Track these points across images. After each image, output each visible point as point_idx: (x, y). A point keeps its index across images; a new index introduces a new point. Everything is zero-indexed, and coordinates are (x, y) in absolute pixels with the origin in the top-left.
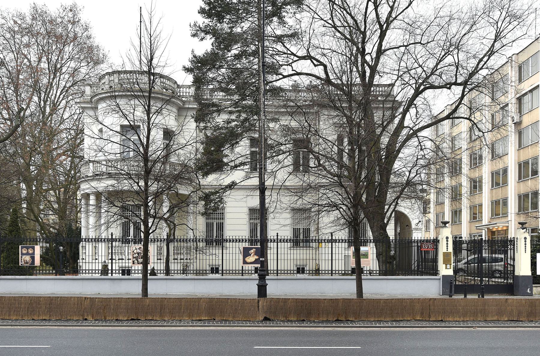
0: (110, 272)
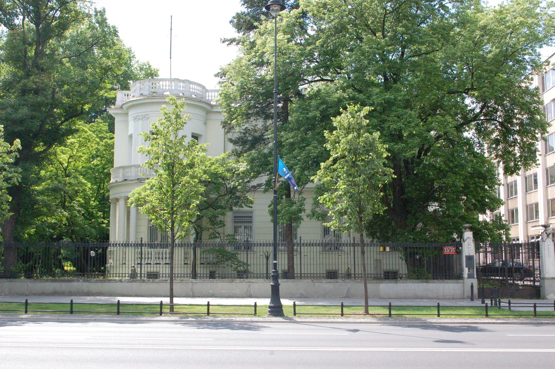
0: (139, 275)
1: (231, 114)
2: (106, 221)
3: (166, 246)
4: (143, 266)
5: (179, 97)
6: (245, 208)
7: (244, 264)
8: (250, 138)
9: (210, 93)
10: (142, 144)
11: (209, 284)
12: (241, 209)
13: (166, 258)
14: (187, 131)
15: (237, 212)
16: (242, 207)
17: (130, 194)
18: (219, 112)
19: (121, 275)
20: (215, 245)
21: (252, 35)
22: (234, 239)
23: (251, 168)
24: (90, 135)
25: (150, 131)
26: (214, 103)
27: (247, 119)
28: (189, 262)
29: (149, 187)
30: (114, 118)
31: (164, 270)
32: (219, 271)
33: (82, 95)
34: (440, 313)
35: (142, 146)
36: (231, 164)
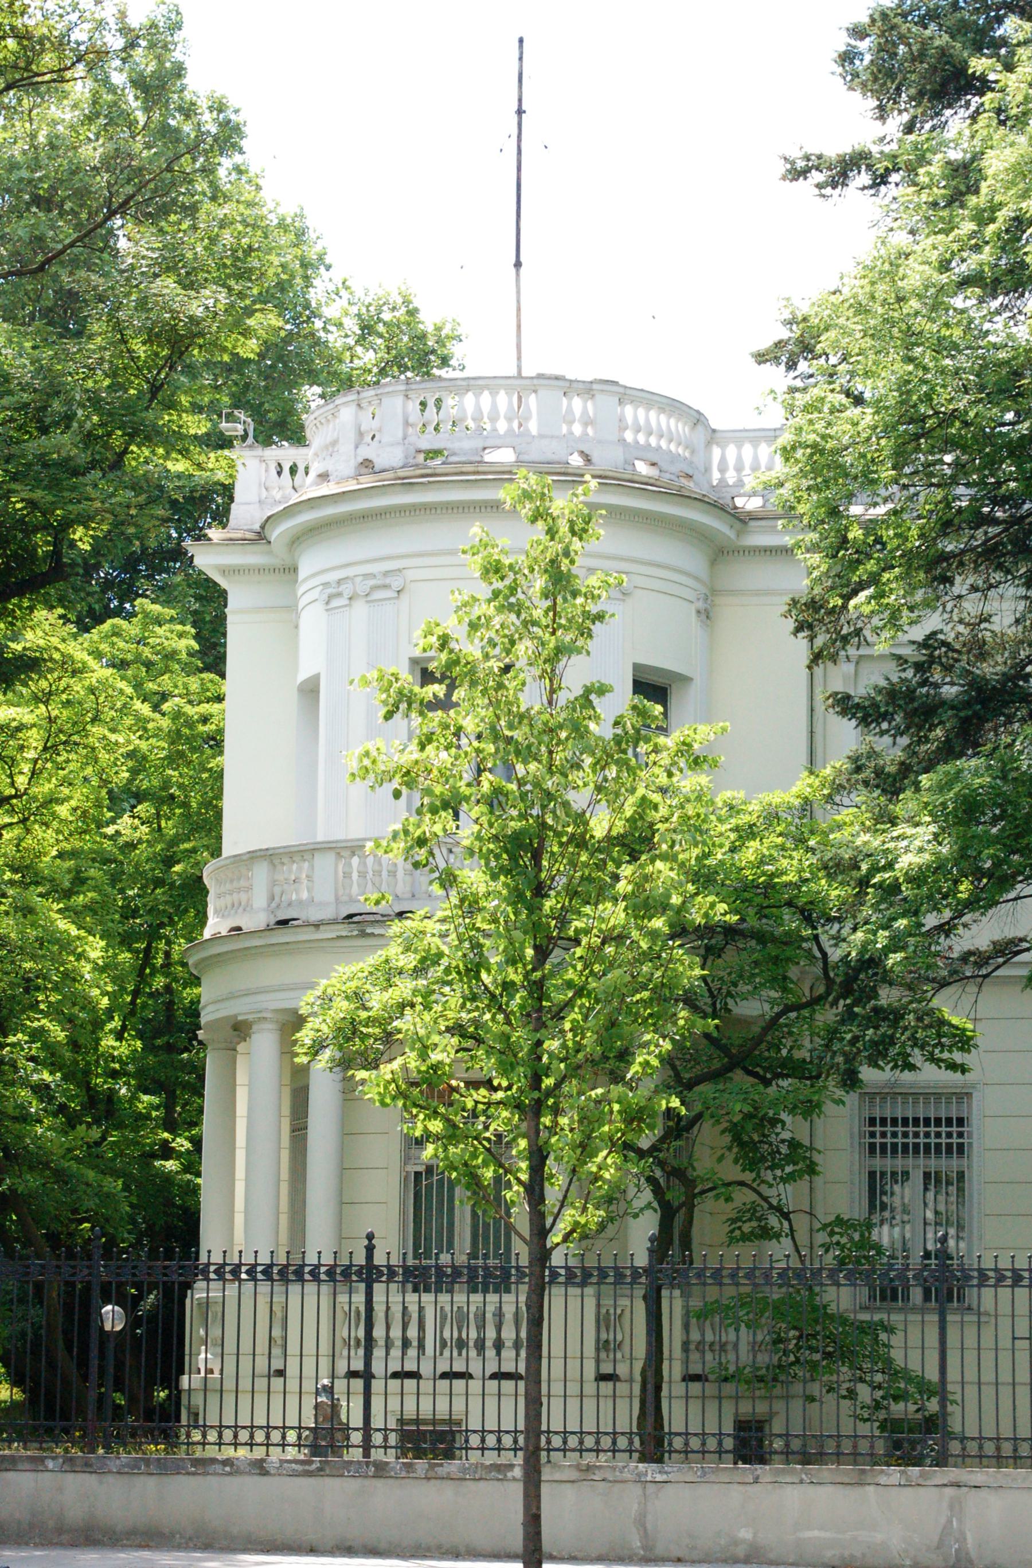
0: (356, 1438)
1: (851, 560)
2: (182, 1144)
3: (499, 1280)
4: (377, 1385)
5: (570, 478)
6: (930, 1075)
7: (925, 1389)
8: (949, 691)
9: (731, 452)
10: (370, 737)
11: (736, 1492)
12: (907, 1076)
13: (499, 1345)
14: (605, 663)
15: (884, 1096)
16: (912, 1067)
17: (310, 996)
18: (787, 551)
19: (260, 1437)
20: (767, 1276)
21: (957, 128)
22: (865, 1243)
23: (962, 855)
24: (103, 682)
25: (414, 661)
26: (754, 504)
27: (929, 584)
28: (622, 1370)
29: (410, 961)
30: (225, 592)
31: (489, 1409)
32: (786, 1418)
33: (62, 473)
35: (370, 746)
36: (847, 832)
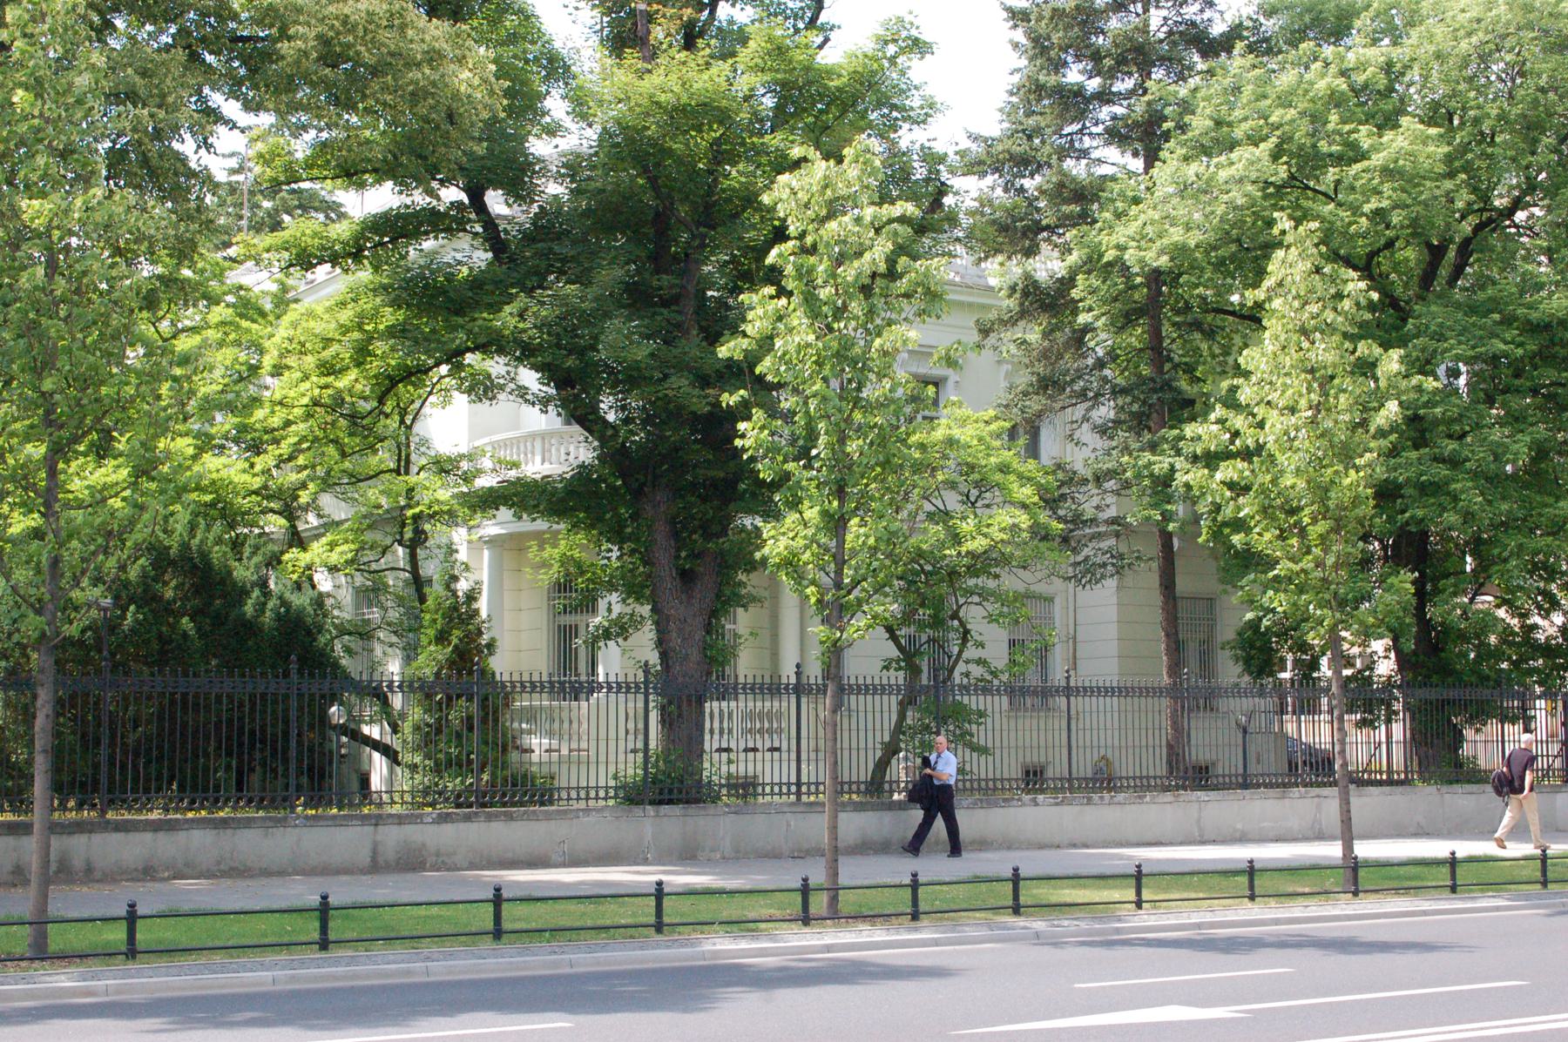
34: (1144, 897)
